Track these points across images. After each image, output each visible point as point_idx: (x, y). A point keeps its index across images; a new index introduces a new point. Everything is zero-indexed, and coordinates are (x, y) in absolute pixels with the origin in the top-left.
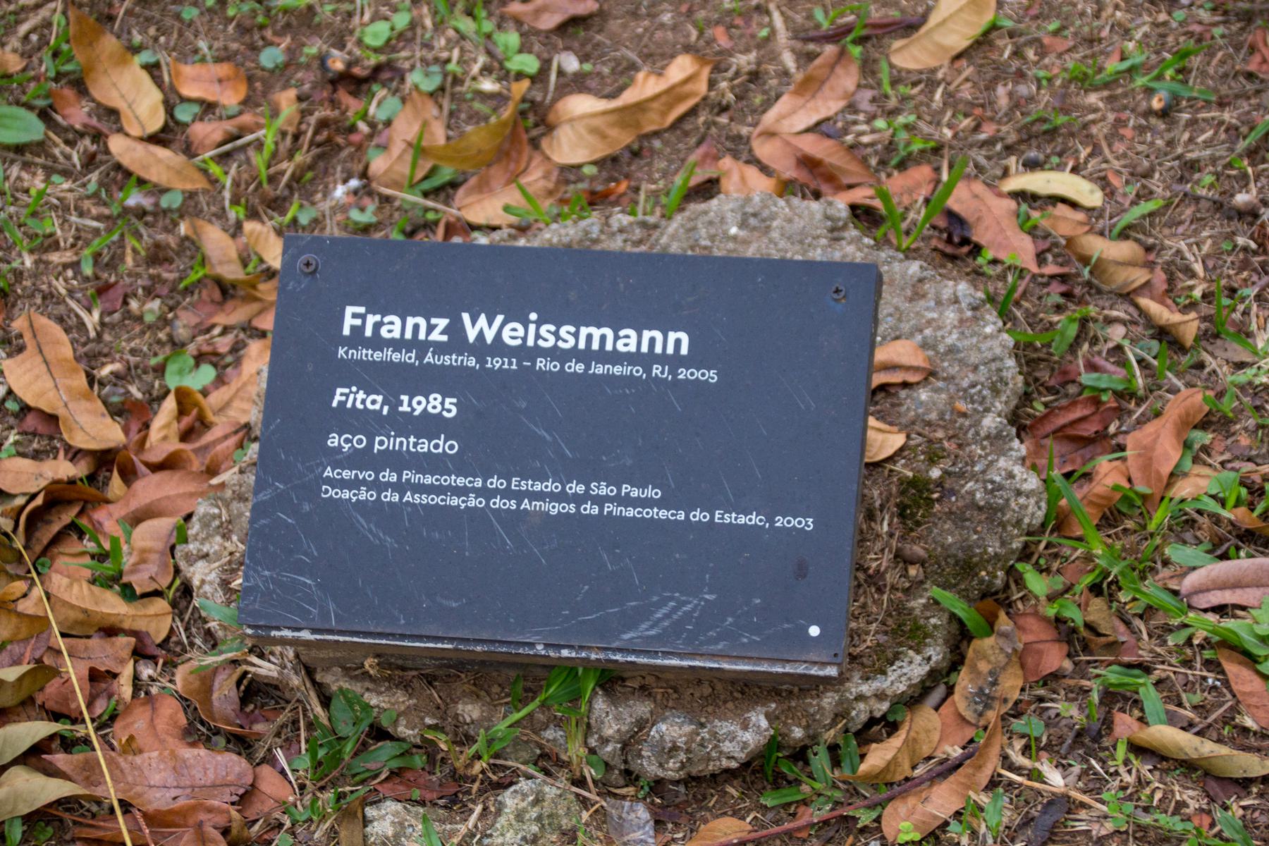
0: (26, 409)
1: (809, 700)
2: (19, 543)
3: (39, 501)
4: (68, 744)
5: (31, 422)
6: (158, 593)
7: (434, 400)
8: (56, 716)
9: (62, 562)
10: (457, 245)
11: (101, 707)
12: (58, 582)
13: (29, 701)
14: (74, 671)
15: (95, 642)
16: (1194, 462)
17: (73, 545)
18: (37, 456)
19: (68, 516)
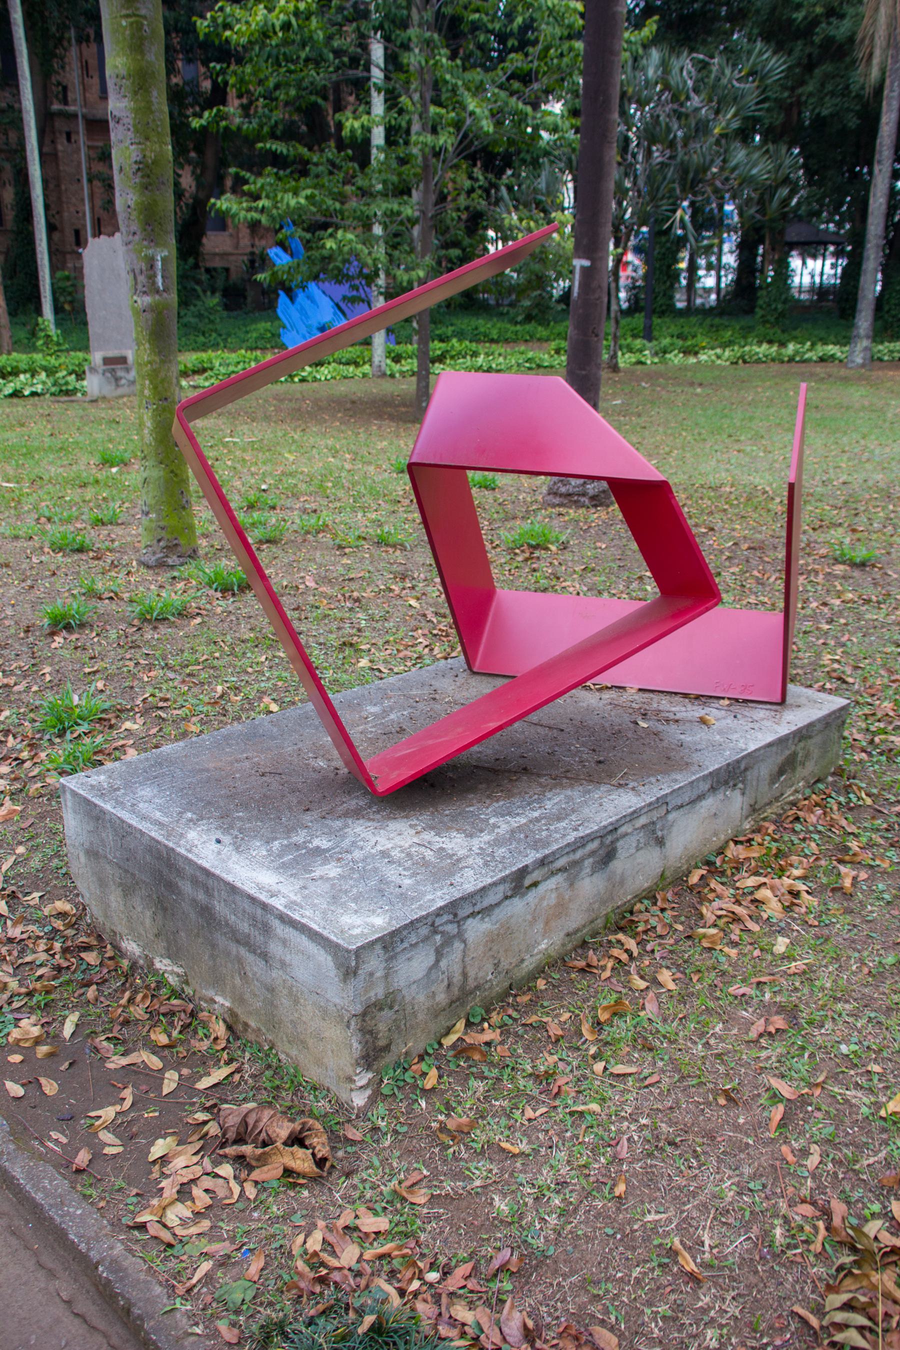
0: (893, 1218)
1: (487, 126)
2: (878, 1259)
3: (888, 1249)
4: (871, 1330)
5: (894, 1223)
6: (840, 525)
7: (772, 273)
8: (870, 1319)
9: (888, 1271)
10: (757, 250)
11: (885, 1325)
12: (885, 1277)
13: (864, 1309)
14: (881, 1308)
15: (889, 1302)
16: (413, 469)
17: (892, 1267)
18: (892, 1233)
19: (895, 1258)
